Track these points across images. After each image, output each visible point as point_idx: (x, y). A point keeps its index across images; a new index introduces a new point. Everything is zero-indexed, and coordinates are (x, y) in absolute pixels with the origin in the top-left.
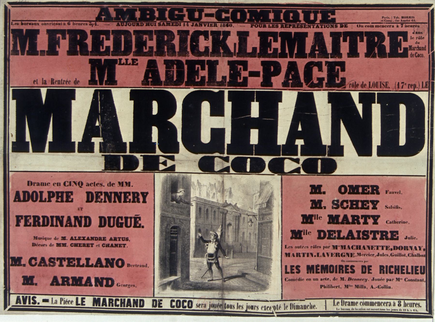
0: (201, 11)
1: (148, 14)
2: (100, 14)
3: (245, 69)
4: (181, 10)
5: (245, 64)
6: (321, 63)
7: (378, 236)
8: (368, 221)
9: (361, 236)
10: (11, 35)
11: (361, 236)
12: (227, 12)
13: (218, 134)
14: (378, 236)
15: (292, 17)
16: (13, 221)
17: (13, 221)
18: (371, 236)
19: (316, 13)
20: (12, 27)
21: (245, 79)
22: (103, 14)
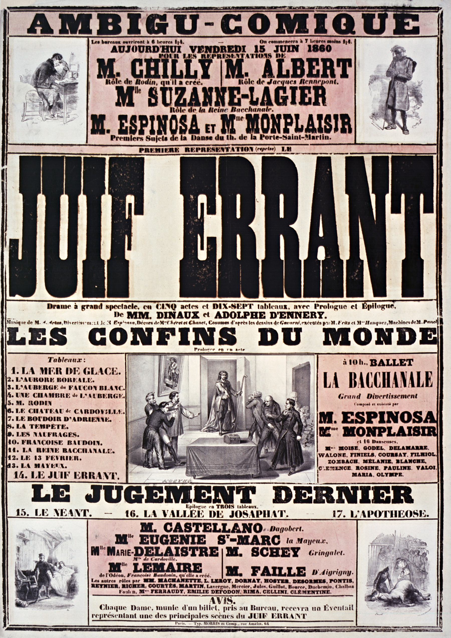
0: (194, 19)
1: (110, 24)
2: (34, 24)
3: (239, 93)
4: (163, 18)
5: (238, 89)
6: (174, 329)
7: (197, 553)
8: (287, 572)
9: (180, 552)
10: (8, 333)
11: (180, 552)
12: (238, 18)
13: (141, 71)
14: (197, 553)
15: (344, 24)
16: (434, 379)
17: (434, 379)
18: (190, 553)
19: (383, 18)
20: (9, 325)
21: (239, 100)
22: (38, 23)
